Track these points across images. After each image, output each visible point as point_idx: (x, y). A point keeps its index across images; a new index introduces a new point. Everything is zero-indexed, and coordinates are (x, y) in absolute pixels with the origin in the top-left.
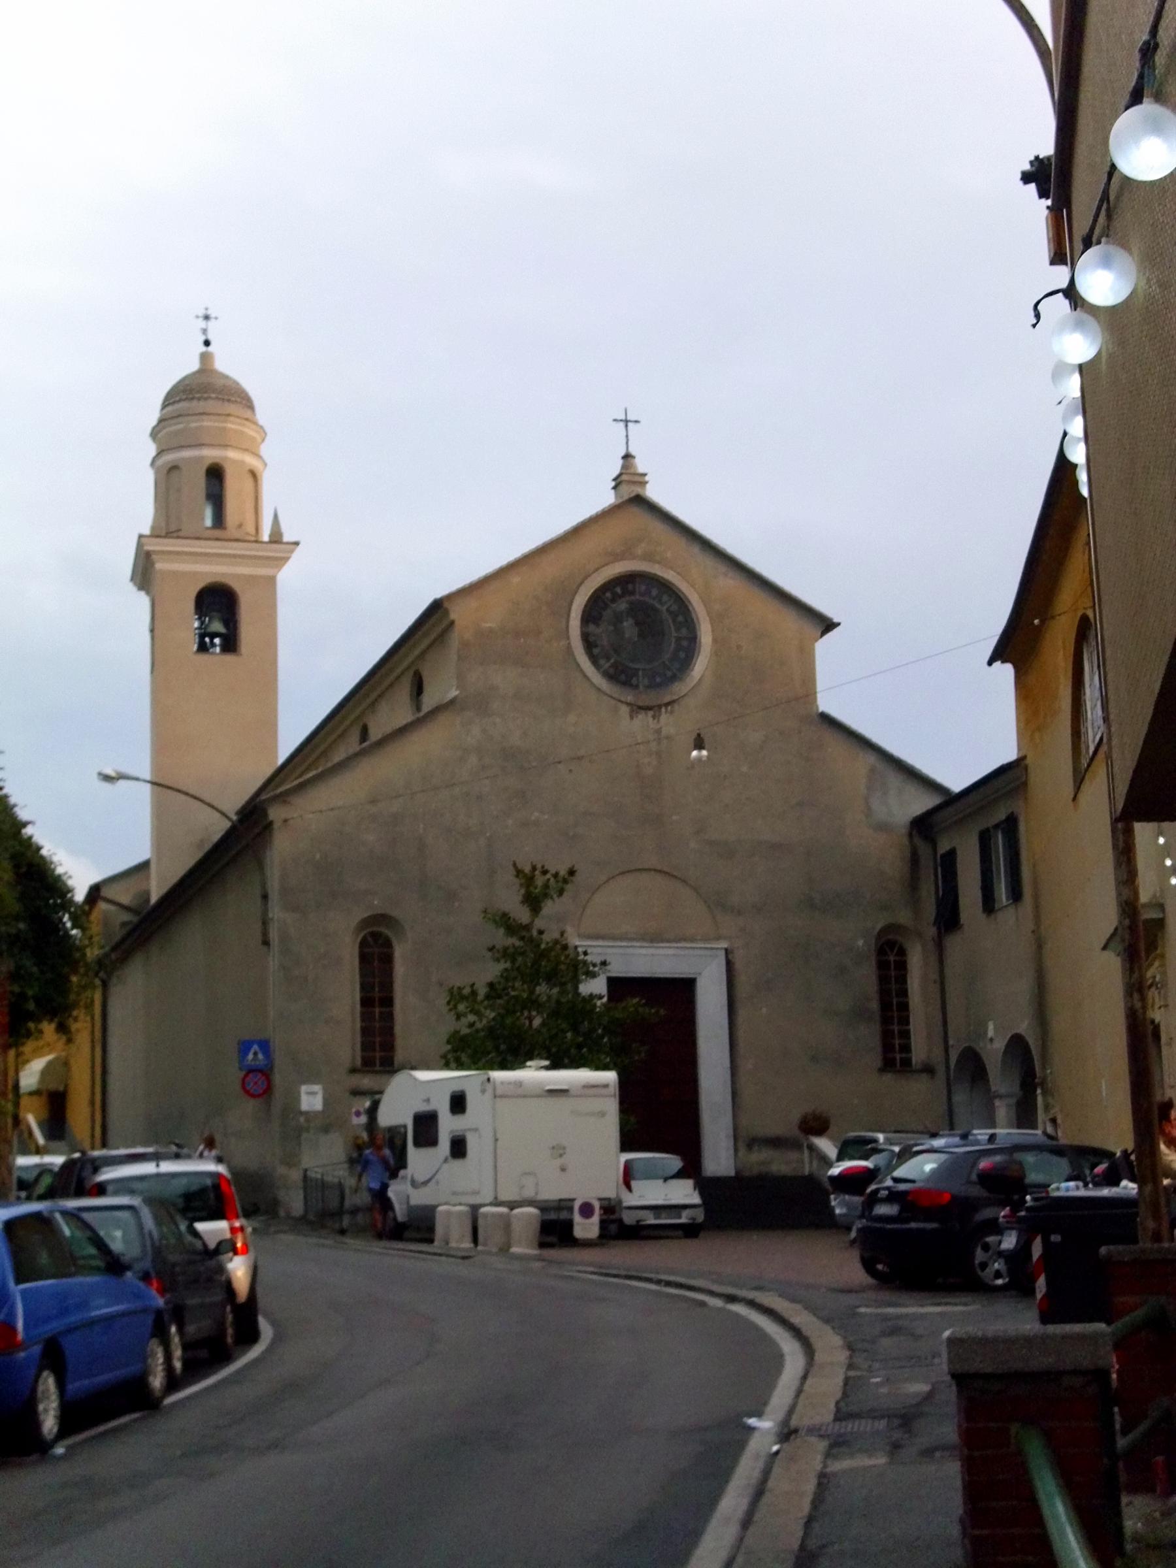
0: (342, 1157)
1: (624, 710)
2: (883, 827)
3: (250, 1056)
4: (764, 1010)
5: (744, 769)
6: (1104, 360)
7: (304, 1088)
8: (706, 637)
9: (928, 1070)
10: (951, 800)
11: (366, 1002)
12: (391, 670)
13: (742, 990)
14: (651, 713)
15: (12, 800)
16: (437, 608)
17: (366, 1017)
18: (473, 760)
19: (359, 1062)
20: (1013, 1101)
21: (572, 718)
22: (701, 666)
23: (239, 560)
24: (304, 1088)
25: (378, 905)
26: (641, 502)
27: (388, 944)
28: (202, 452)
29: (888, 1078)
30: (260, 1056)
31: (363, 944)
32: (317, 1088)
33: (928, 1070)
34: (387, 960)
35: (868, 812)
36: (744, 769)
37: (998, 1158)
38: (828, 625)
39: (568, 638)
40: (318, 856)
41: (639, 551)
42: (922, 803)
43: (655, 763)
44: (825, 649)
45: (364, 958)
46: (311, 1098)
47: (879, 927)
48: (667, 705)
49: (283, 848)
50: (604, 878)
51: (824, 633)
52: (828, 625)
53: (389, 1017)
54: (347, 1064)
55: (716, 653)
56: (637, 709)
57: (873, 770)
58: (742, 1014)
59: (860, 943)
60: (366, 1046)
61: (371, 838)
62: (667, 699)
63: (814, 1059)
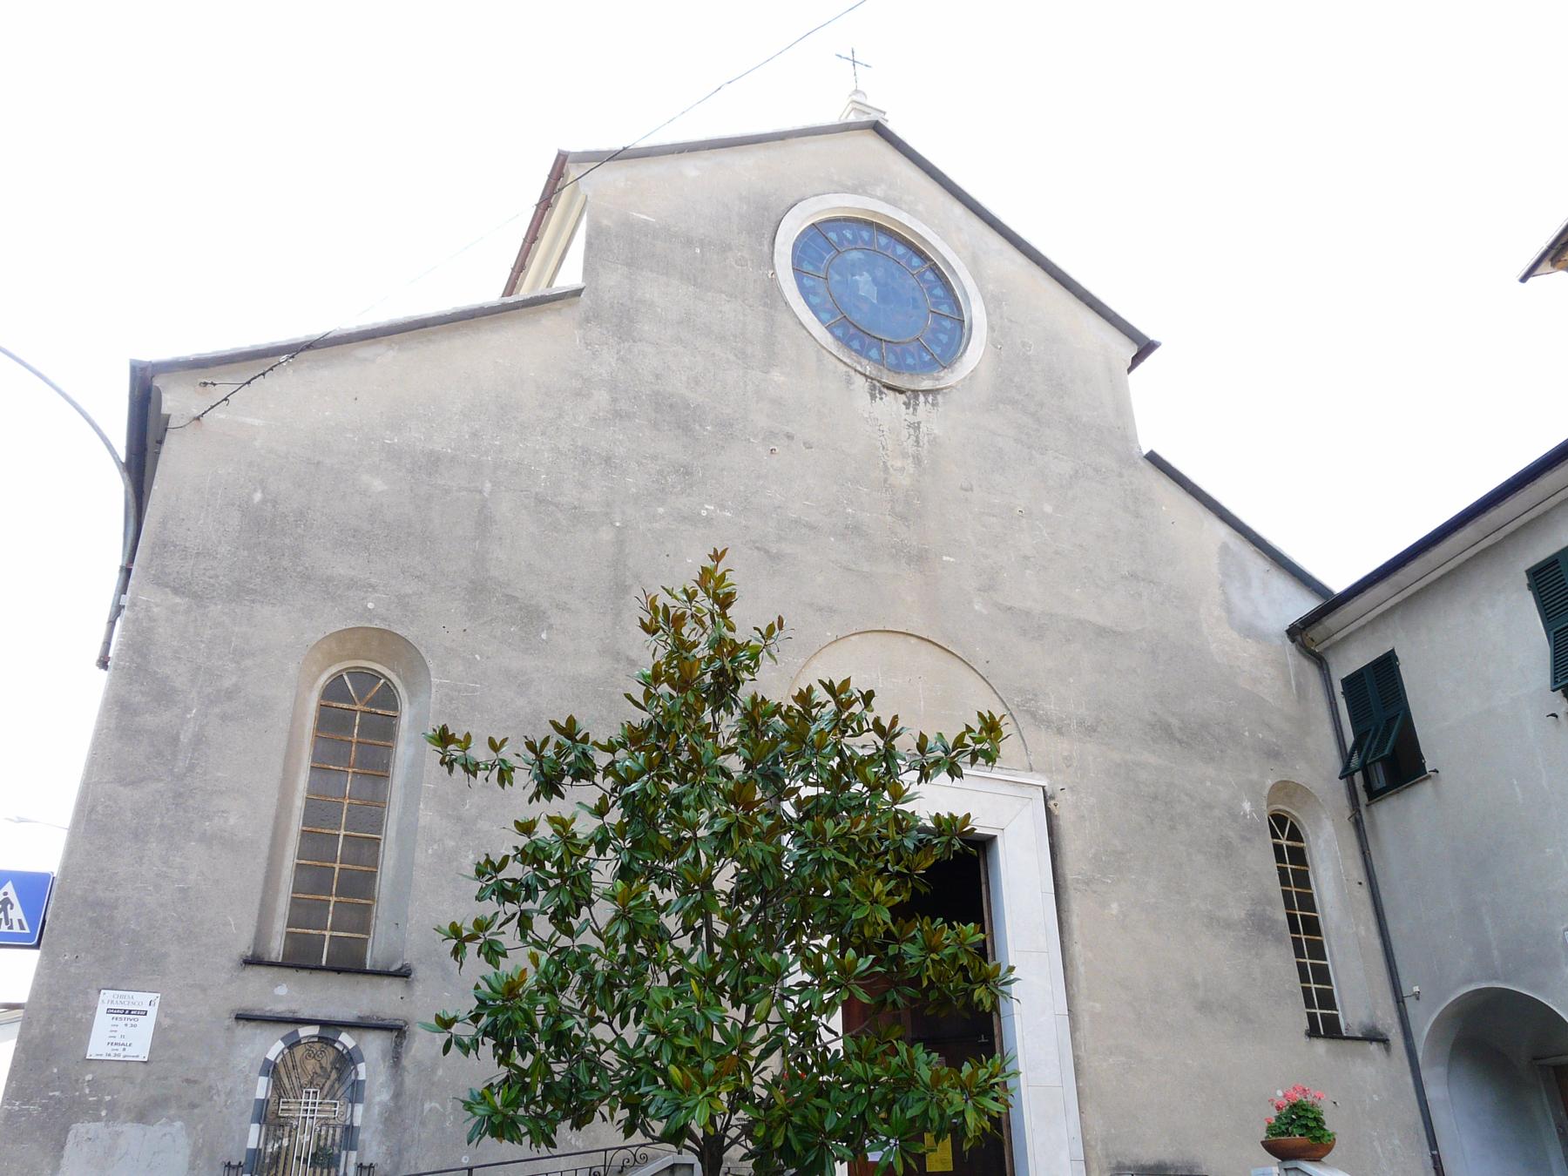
4: (1114, 906)
7: (107, 998)
8: (976, 312)
10: (1332, 604)
13: (1073, 868)
14: (903, 398)
15: (506, 1142)
18: (602, 397)
19: (276, 948)
21: (776, 376)
22: (975, 353)
25: (375, 608)
27: (388, 698)
28: (980, 714)
31: (334, 690)
33: (1374, 1036)
36: (1048, 509)
37: (585, 218)
38: (1145, 348)
39: (773, 267)
40: (258, 497)
41: (879, 192)
45: (331, 721)
46: (122, 1022)
47: (1270, 782)
48: (926, 392)
50: (830, 636)
51: (1137, 360)
56: (880, 388)
57: (1224, 549)
58: (1077, 905)
61: (378, 485)
63: (1204, 1007)
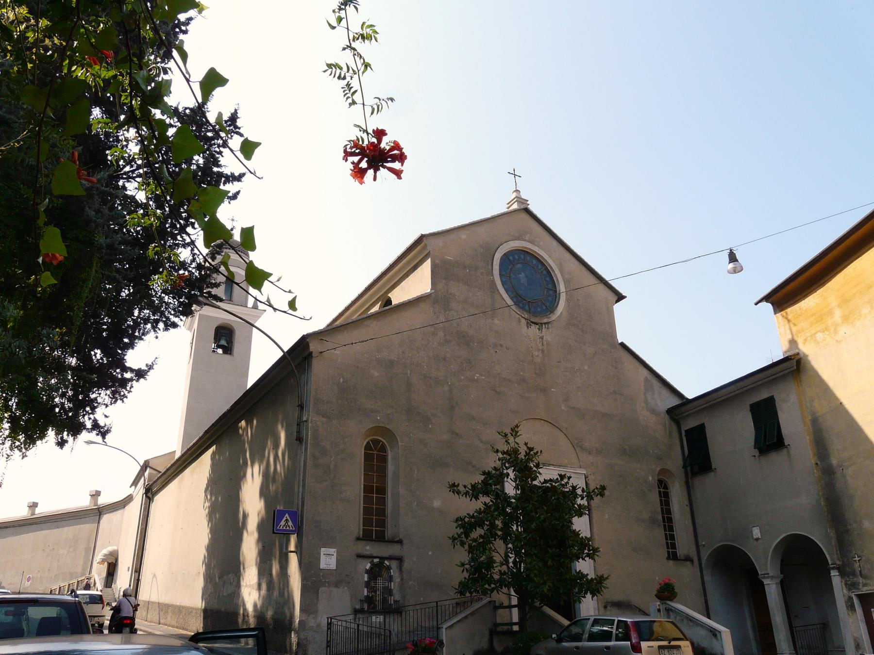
0: (349, 610)
1: (523, 321)
2: (653, 412)
3: (283, 523)
5: (586, 368)
6: (249, 463)
8: (562, 287)
9: (688, 559)
10: (686, 402)
11: (368, 489)
12: (409, 262)
16: (422, 238)
17: (367, 500)
20: (778, 581)
23: (19, 529)
24: (323, 550)
26: (527, 211)
27: (383, 449)
29: (671, 563)
30: (290, 523)
31: (367, 447)
32: (333, 551)
33: (688, 559)
34: (383, 460)
35: (646, 402)
36: (586, 368)
38: (620, 297)
42: (676, 402)
43: (541, 355)
44: (618, 308)
45: (368, 458)
48: (545, 323)
49: (319, 370)
51: (617, 301)
52: (620, 297)
53: (382, 502)
54: (355, 535)
55: (567, 300)
57: (646, 379)
59: (650, 478)
60: (367, 522)
61: (376, 374)
62: (545, 320)
